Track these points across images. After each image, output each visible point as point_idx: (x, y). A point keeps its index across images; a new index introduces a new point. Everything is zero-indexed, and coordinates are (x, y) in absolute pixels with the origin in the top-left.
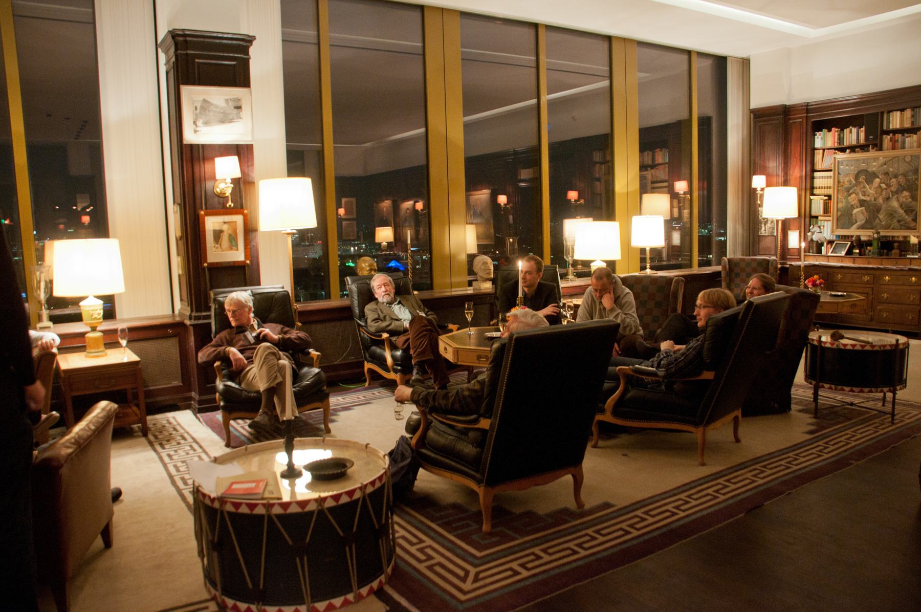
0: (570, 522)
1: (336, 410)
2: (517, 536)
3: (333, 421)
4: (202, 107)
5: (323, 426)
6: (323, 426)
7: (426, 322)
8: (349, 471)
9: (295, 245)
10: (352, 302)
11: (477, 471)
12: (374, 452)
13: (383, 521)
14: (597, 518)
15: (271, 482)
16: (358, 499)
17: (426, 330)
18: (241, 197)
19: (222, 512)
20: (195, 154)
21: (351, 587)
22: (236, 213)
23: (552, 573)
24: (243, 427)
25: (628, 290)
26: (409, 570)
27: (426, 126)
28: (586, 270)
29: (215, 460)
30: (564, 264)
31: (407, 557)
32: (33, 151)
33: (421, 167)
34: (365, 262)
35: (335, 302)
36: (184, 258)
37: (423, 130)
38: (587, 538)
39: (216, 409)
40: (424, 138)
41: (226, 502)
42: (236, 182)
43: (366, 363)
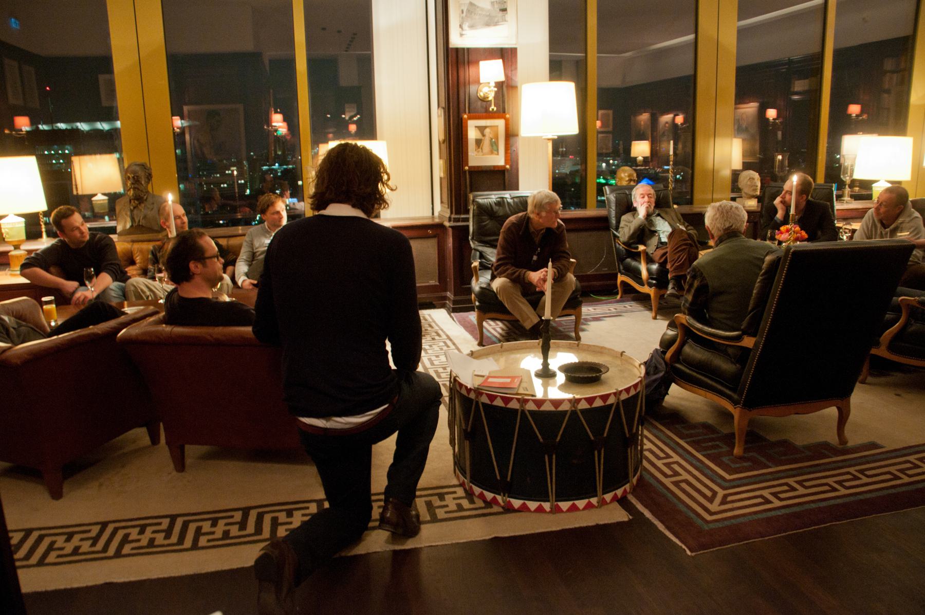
0: (829, 457)
1: (586, 320)
2: (770, 464)
3: (583, 330)
4: (468, 11)
5: (573, 334)
6: (573, 334)
7: (686, 236)
8: (603, 376)
9: (555, 153)
10: (609, 212)
11: (734, 390)
12: (629, 361)
13: (634, 431)
14: (861, 457)
15: (525, 379)
16: (612, 405)
17: (686, 244)
18: (503, 102)
19: (477, 402)
20: (460, 57)
21: (596, 491)
22: (499, 118)
23: (807, 507)
24: (494, 329)
25: (917, 214)
26: (652, 481)
27: (696, 32)
28: (864, 192)
29: (472, 354)
30: (841, 185)
31: (653, 470)
32: (311, 62)
33: (687, 78)
34: (624, 172)
35: (591, 211)
36: (446, 163)
37: (692, 36)
38: (849, 477)
39: (472, 309)
40: (693, 46)
41: (482, 394)
42: (500, 85)
43: (619, 275)
